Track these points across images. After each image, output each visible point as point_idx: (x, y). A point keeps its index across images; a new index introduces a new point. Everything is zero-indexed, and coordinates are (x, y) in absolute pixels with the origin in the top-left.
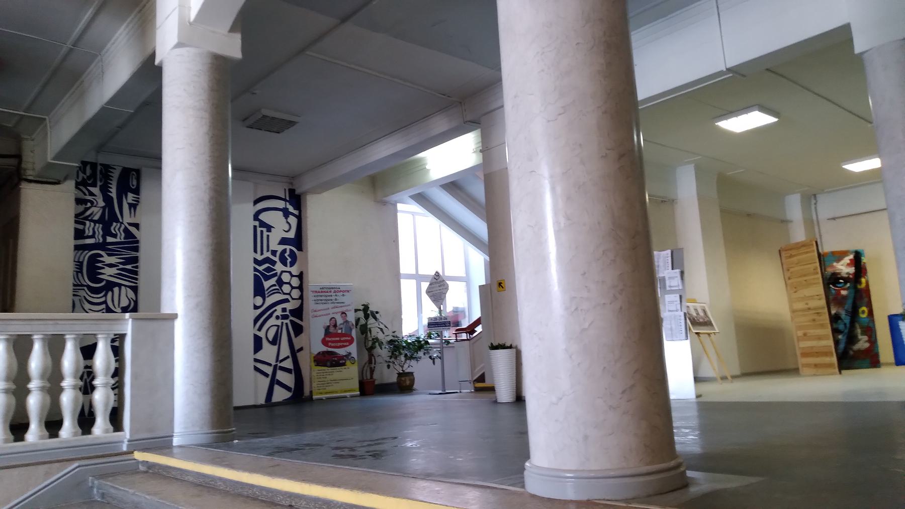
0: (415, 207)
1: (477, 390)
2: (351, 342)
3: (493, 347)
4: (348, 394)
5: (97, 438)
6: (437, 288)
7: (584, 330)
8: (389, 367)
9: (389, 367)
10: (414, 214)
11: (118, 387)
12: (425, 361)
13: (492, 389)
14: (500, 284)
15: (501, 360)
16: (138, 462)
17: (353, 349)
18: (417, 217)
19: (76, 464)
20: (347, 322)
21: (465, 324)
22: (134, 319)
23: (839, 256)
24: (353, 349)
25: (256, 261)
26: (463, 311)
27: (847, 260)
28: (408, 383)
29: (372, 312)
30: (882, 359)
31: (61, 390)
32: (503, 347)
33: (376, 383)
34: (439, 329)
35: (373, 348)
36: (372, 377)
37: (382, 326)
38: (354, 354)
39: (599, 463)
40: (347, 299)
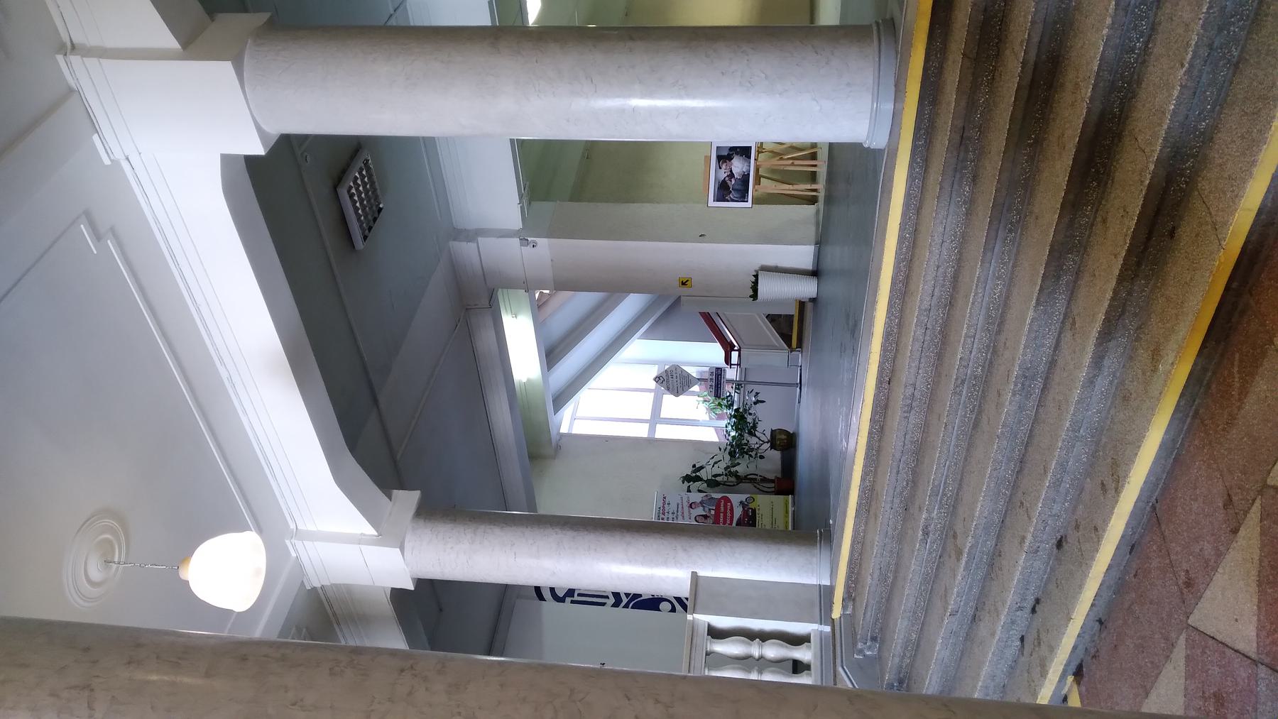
0: (567, 412)
1: (800, 345)
2: (727, 500)
3: (755, 296)
4: (791, 509)
5: (815, 655)
6: (673, 381)
7: (766, 77)
8: (762, 457)
9: (762, 457)
10: (574, 419)
11: (764, 637)
12: (759, 410)
13: (802, 305)
14: (683, 284)
15: (769, 288)
16: (843, 615)
17: (736, 499)
18: (579, 414)
19: (840, 670)
20: (701, 503)
22: (694, 612)
24: (736, 499)
25: (616, 605)
28: (783, 437)
29: (694, 472)
31: (761, 657)
32: (756, 283)
33: (779, 475)
35: (736, 475)
36: (772, 481)
37: (712, 462)
38: (743, 497)
39: (869, 76)
40: (674, 500)
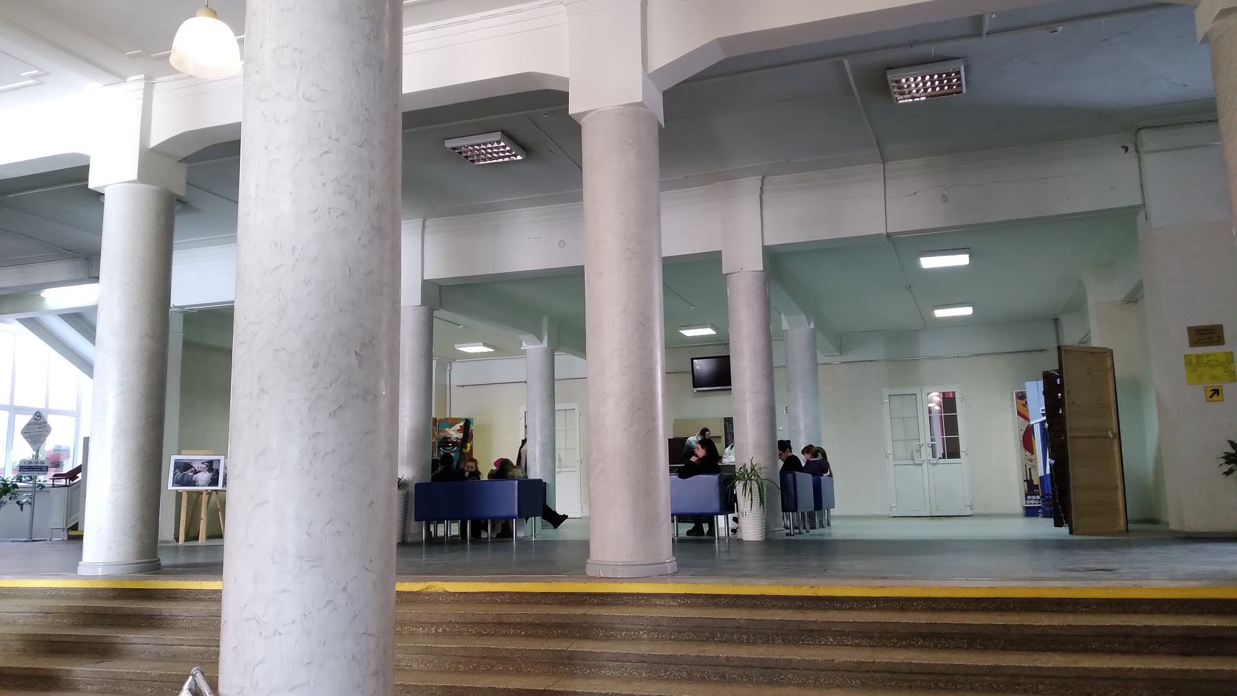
21: (67, 468)
23: (452, 422)
26: (67, 451)
27: (458, 426)
30: (1125, 197)
34: (32, 474)
